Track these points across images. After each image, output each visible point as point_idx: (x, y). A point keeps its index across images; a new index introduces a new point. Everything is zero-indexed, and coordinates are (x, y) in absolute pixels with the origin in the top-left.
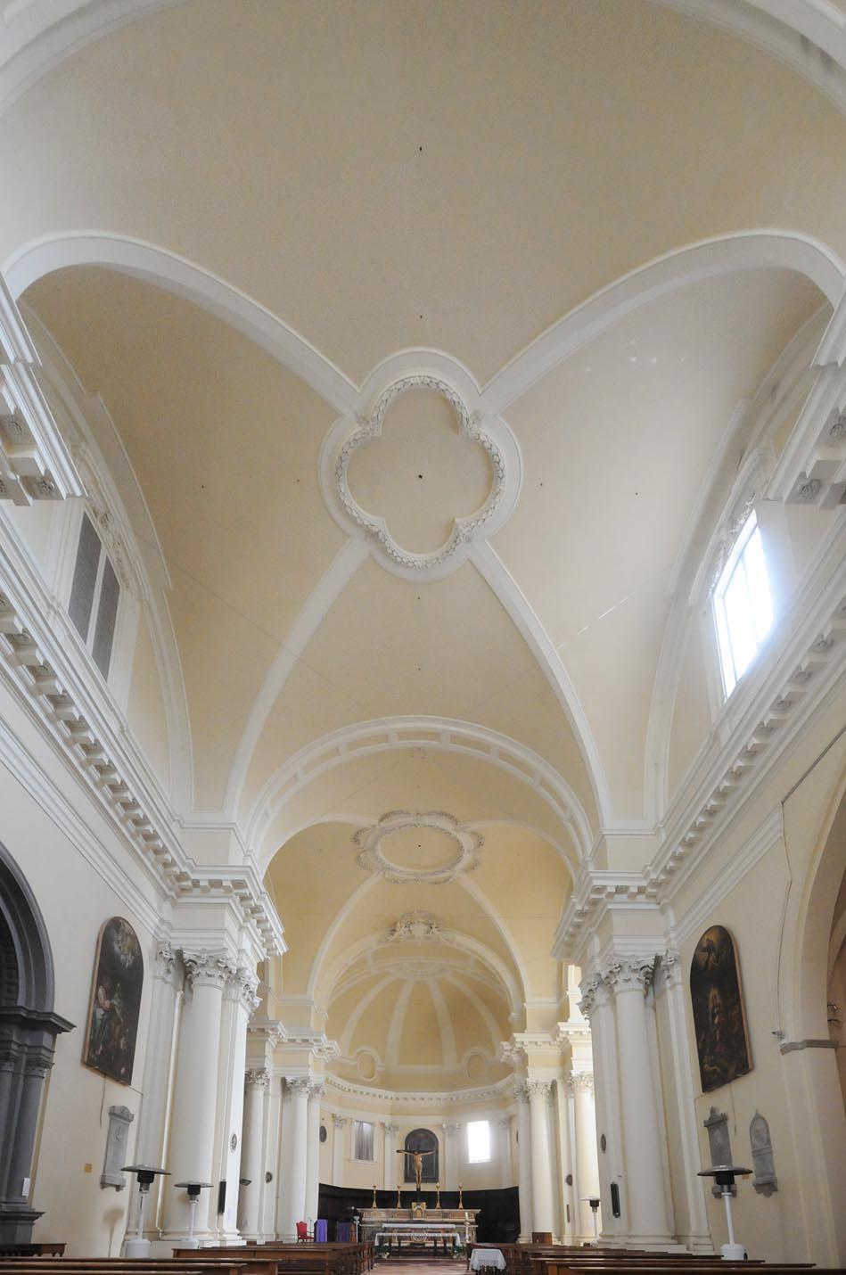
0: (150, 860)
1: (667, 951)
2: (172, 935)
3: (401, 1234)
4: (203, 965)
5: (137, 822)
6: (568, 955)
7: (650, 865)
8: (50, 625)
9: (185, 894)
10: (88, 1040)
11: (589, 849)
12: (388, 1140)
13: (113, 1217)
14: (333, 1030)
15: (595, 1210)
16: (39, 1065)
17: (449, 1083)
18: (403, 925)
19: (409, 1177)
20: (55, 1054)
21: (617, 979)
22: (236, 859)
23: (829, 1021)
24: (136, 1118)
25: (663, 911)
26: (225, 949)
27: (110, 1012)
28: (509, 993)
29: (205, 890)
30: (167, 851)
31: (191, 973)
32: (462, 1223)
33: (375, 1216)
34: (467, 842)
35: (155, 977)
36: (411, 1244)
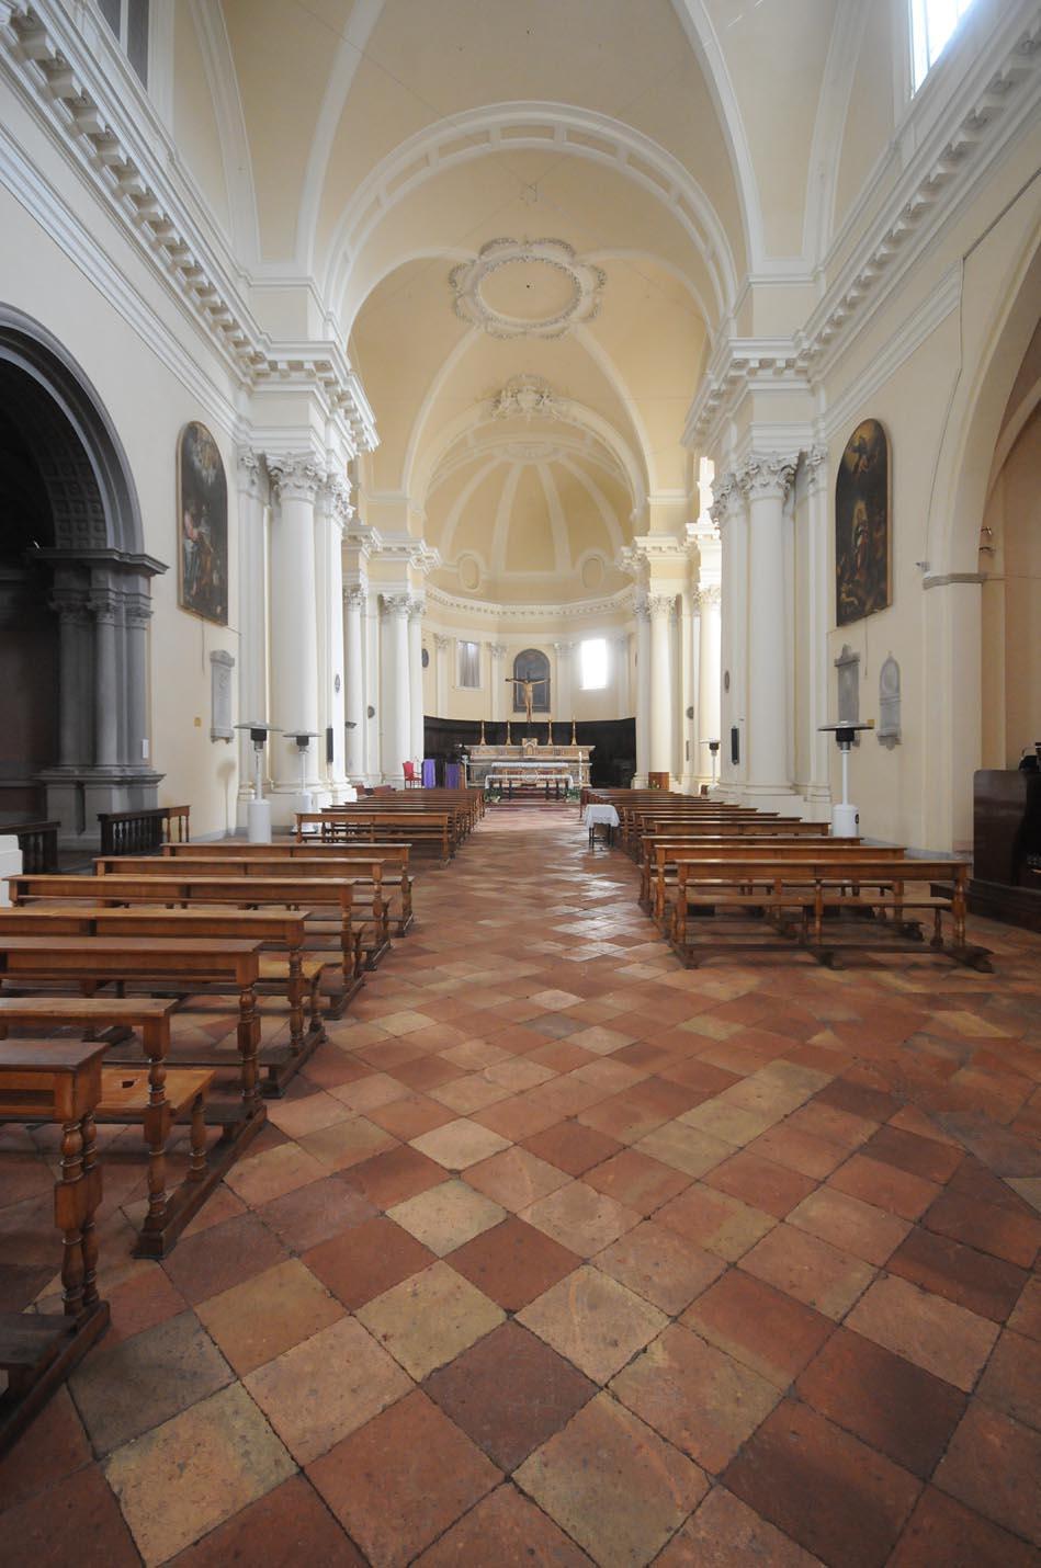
0: (219, 339)
1: (814, 447)
2: (252, 434)
3: (512, 776)
4: (290, 474)
5: (202, 291)
6: (700, 445)
7: (804, 330)
8: (79, 28)
9: (261, 380)
10: (181, 580)
11: (733, 301)
12: (495, 663)
13: (226, 769)
14: (432, 539)
15: (714, 754)
16: (139, 615)
17: (560, 593)
18: (509, 394)
19: (518, 706)
20: (152, 601)
21: (753, 483)
22: (316, 332)
23: (981, 549)
24: (237, 662)
25: (813, 391)
26: (313, 453)
27: (199, 542)
28: (630, 480)
29: (284, 375)
30: (238, 327)
31: (277, 483)
32: (576, 761)
33: (482, 753)
34: (586, 280)
35: (239, 492)
36: (523, 785)
